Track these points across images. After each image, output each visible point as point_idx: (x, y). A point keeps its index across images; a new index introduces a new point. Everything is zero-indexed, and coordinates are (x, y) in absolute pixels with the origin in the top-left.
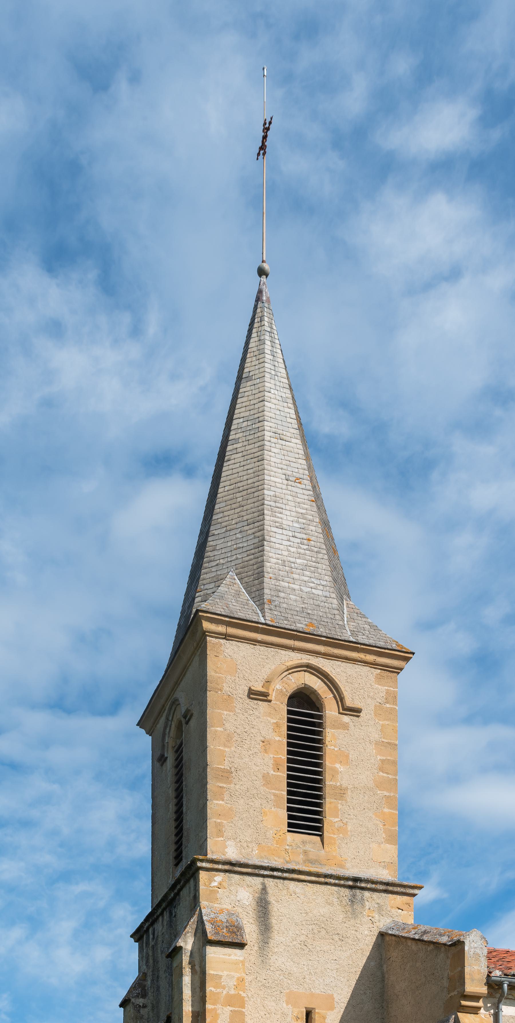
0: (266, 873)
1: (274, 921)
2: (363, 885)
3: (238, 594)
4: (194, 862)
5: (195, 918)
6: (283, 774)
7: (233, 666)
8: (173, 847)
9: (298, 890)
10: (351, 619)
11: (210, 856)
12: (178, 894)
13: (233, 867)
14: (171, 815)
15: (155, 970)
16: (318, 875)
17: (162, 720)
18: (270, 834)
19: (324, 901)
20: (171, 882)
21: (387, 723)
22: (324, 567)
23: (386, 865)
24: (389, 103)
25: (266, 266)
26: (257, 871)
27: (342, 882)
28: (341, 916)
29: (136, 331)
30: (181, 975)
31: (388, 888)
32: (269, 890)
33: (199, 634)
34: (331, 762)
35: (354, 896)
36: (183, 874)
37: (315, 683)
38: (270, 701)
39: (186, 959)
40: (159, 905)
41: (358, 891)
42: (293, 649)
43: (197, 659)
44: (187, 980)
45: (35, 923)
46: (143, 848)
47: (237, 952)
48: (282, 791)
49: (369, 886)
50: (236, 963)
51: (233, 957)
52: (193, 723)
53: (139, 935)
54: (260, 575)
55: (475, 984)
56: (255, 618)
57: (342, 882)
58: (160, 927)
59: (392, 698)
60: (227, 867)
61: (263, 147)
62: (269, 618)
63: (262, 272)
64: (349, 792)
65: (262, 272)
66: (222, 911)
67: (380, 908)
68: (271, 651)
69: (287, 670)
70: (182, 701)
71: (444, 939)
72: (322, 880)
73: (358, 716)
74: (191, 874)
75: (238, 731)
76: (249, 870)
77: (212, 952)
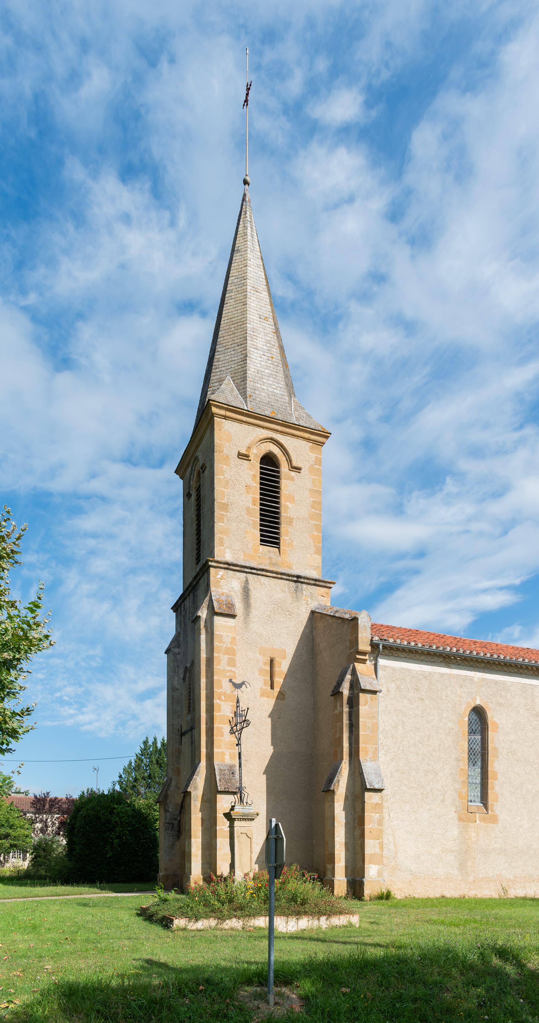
0: (248, 570)
1: (252, 601)
2: (302, 580)
3: (232, 390)
4: (207, 561)
5: (207, 598)
6: (258, 507)
7: (231, 437)
8: (195, 552)
9: (266, 583)
10: (296, 410)
11: (216, 559)
12: (198, 582)
13: (229, 566)
14: (194, 531)
16: (277, 573)
17: (189, 470)
20: (194, 574)
24: (315, 89)
25: (248, 179)
26: (242, 569)
27: (290, 578)
28: (290, 600)
29: (173, 223)
30: (200, 634)
31: (316, 583)
36: (201, 569)
37: (276, 450)
38: (250, 460)
39: (202, 624)
41: (299, 584)
44: (203, 637)
49: (306, 581)
51: (229, 624)
53: (176, 608)
54: (244, 379)
55: (364, 646)
57: (290, 578)
58: (188, 603)
59: (318, 461)
62: (250, 407)
63: (246, 182)
65: (246, 182)
66: (223, 594)
67: (312, 595)
70: (200, 458)
71: (347, 616)
72: (279, 576)
73: (300, 472)
74: (204, 570)
76: (238, 568)
77: (218, 620)
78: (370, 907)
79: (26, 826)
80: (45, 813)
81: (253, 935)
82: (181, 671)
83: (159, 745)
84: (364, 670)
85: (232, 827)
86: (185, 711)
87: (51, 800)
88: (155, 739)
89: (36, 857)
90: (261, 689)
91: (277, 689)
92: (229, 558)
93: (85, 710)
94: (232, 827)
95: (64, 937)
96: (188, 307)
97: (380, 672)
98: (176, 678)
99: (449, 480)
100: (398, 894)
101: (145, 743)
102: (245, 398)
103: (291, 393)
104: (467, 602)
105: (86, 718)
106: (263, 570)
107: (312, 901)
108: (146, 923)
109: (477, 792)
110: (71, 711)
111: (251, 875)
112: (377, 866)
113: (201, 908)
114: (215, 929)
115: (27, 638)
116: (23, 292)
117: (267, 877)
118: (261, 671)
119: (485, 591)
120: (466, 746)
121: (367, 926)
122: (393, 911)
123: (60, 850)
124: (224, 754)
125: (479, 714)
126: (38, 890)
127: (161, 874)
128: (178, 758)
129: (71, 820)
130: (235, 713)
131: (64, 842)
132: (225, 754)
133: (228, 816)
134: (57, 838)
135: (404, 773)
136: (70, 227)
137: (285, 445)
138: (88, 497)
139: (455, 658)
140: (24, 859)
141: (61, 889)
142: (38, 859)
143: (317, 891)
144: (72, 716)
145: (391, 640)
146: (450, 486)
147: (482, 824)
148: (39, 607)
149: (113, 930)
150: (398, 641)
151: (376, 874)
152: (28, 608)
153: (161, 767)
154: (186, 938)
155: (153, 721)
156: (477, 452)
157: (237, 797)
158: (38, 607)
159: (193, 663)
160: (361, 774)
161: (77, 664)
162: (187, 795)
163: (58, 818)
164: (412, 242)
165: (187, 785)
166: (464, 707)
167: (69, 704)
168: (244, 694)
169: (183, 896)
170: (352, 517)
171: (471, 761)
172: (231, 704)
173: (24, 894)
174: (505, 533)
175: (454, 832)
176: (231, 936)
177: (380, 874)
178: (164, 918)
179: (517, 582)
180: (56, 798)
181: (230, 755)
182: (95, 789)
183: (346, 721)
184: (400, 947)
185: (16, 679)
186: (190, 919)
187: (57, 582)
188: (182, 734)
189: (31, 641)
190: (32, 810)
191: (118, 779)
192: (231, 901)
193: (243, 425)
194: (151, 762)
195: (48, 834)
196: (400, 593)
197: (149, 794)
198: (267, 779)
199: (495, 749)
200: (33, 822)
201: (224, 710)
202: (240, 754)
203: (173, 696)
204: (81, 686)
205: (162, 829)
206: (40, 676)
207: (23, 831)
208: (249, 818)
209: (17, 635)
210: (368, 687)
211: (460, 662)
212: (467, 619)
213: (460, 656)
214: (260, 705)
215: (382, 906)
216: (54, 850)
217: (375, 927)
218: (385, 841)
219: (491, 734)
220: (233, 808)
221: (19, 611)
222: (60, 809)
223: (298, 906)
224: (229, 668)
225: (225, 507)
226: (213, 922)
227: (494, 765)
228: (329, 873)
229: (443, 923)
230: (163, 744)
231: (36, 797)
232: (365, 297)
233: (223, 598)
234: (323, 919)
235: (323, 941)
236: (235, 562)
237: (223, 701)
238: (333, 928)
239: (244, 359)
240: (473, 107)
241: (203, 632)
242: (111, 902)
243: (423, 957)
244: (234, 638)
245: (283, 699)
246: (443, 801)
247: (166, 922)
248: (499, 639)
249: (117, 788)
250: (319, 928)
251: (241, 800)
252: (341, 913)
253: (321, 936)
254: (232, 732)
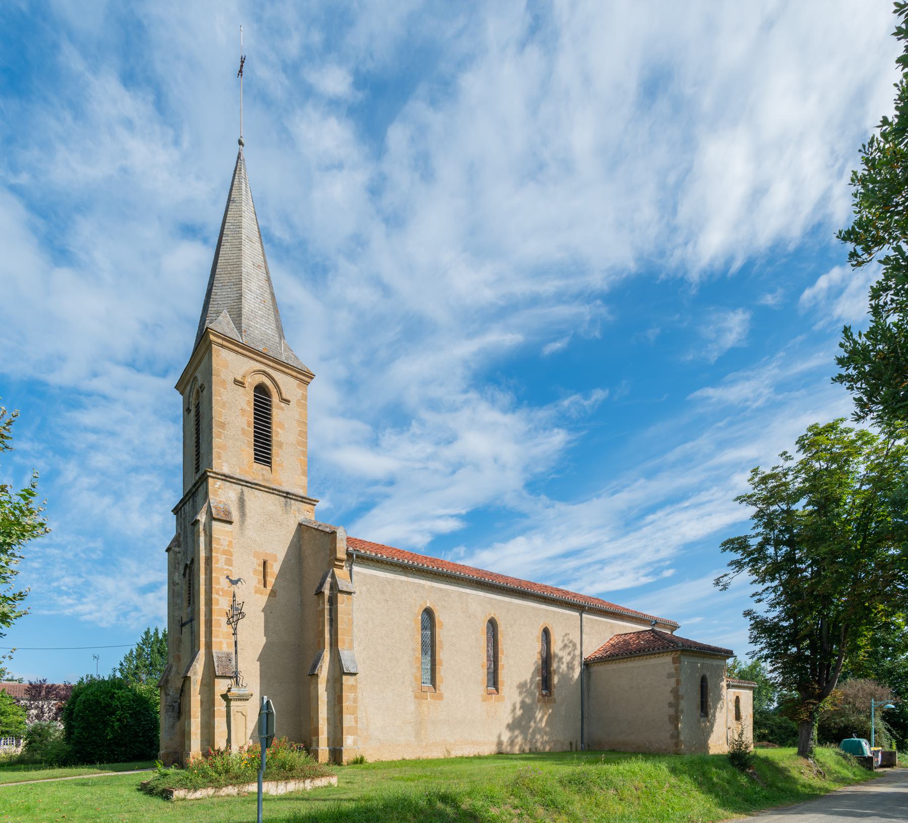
1: (247, 511)
3: (228, 323)
4: (206, 472)
5: (206, 505)
6: (252, 430)
7: (227, 365)
8: (195, 462)
10: (285, 350)
11: (214, 470)
12: (197, 489)
13: (226, 478)
14: (193, 444)
15: (185, 532)
16: (269, 488)
17: (189, 388)
18: (245, 462)
19: (273, 503)
20: (194, 482)
22: (272, 318)
23: (303, 488)
24: (311, 56)
25: (243, 140)
28: (280, 513)
29: (177, 142)
30: (199, 536)
31: (303, 499)
33: (208, 342)
34: (275, 427)
36: (200, 478)
37: (268, 383)
39: (201, 527)
40: (187, 495)
43: (207, 355)
44: (202, 539)
45: (118, 496)
46: (179, 459)
47: (228, 525)
48: (252, 440)
50: (228, 532)
52: (205, 392)
53: (177, 511)
54: (240, 315)
55: (341, 555)
56: (237, 339)
58: (187, 507)
59: (305, 397)
61: (241, 71)
62: (244, 340)
63: (240, 143)
65: (240, 143)
66: (220, 502)
67: (299, 510)
70: (199, 378)
71: (328, 530)
74: (204, 479)
77: (215, 524)
78: (347, 770)
79: (20, 713)
80: (41, 700)
81: (244, 799)
82: (182, 568)
83: (160, 636)
84: (341, 574)
85: (228, 706)
86: (185, 604)
87: (47, 687)
88: (157, 630)
89: (30, 743)
90: (255, 587)
91: (269, 588)
92: (226, 470)
93: (84, 600)
94: (228, 706)
95: (60, 815)
96: (189, 231)
97: (354, 577)
98: (177, 574)
99: (414, 423)
100: (369, 759)
101: (147, 633)
102: (240, 332)
103: (281, 336)
104: (427, 525)
105: (87, 609)
106: (257, 484)
107: (298, 767)
108: (147, 797)
109: (428, 676)
110: (70, 601)
111: (246, 748)
113: (200, 780)
114: (213, 797)
115: (19, 524)
116: (14, 169)
117: (259, 749)
118: (255, 571)
119: (440, 517)
120: (420, 639)
121: (344, 785)
122: (365, 772)
123: (57, 734)
124: (222, 643)
125: (429, 614)
126: (33, 774)
127: (162, 752)
128: (179, 646)
129: (69, 705)
130: (232, 607)
131: (62, 727)
133: (225, 697)
134: (55, 723)
136: (68, 115)
137: (276, 379)
138: (89, 394)
140: (17, 746)
141: (58, 771)
142: (33, 744)
143: (303, 758)
144: (71, 605)
145: (363, 551)
146: (415, 428)
148: (34, 495)
149: (113, 805)
150: (368, 552)
152: (21, 495)
153: (162, 655)
154: (185, 808)
155: (156, 612)
156: (434, 405)
157: (233, 681)
158: (32, 494)
159: (192, 561)
160: (340, 660)
161: (76, 555)
162: (186, 679)
163: (55, 704)
164: (387, 221)
165: (187, 671)
167: (67, 594)
168: (239, 589)
169: (182, 771)
170: (336, 445)
171: (424, 652)
173: (17, 779)
174: (454, 472)
175: (412, 707)
176: (227, 802)
177: (355, 742)
178: (164, 790)
179: (464, 512)
180: (53, 685)
182: (95, 676)
183: (327, 617)
184: (369, 800)
185: (7, 563)
186: (189, 789)
187: (53, 474)
188: (183, 625)
189: (24, 527)
190: (28, 696)
191: (119, 667)
192: (227, 772)
194: (153, 651)
195: (45, 720)
196: (375, 511)
197: (150, 680)
198: (261, 666)
199: (441, 642)
200: (27, 709)
201: (222, 604)
202: (236, 642)
203: (174, 590)
204: (80, 576)
205: (163, 712)
206: (35, 565)
207: (16, 717)
208: (244, 698)
209: (8, 520)
210: (345, 589)
212: (427, 539)
213: (415, 568)
214: (254, 601)
215: (357, 769)
216: (51, 735)
217: (350, 786)
218: (359, 716)
219: (437, 630)
220: (229, 690)
221: (10, 497)
222: (57, 695)
223: (286, 772)
224: (226, 567)
225: (223, 425)
226: (211, 791)
227: (441, 655)
228: (314, 744)
229: (402, 779)
230: (164, 635)
231: (31, 684)
232: (351, 256)
233: (221, 506)
234: (308, 781)
235: (307, 800)
238: (315, 789)
239: (240, 298)
240: (436, 119)
241: (202, 535)
242: (112, 780)
243: (386, 806)
244: (230, 542)
245: (275, 596)
246: (403, 683)
247: (166, 795)
248: (448, 557)
249: (118, 675)
250: (305, 789)
251: (237, 683)
252: (322, 776)
253: (306, 796)
254: (229, 623)
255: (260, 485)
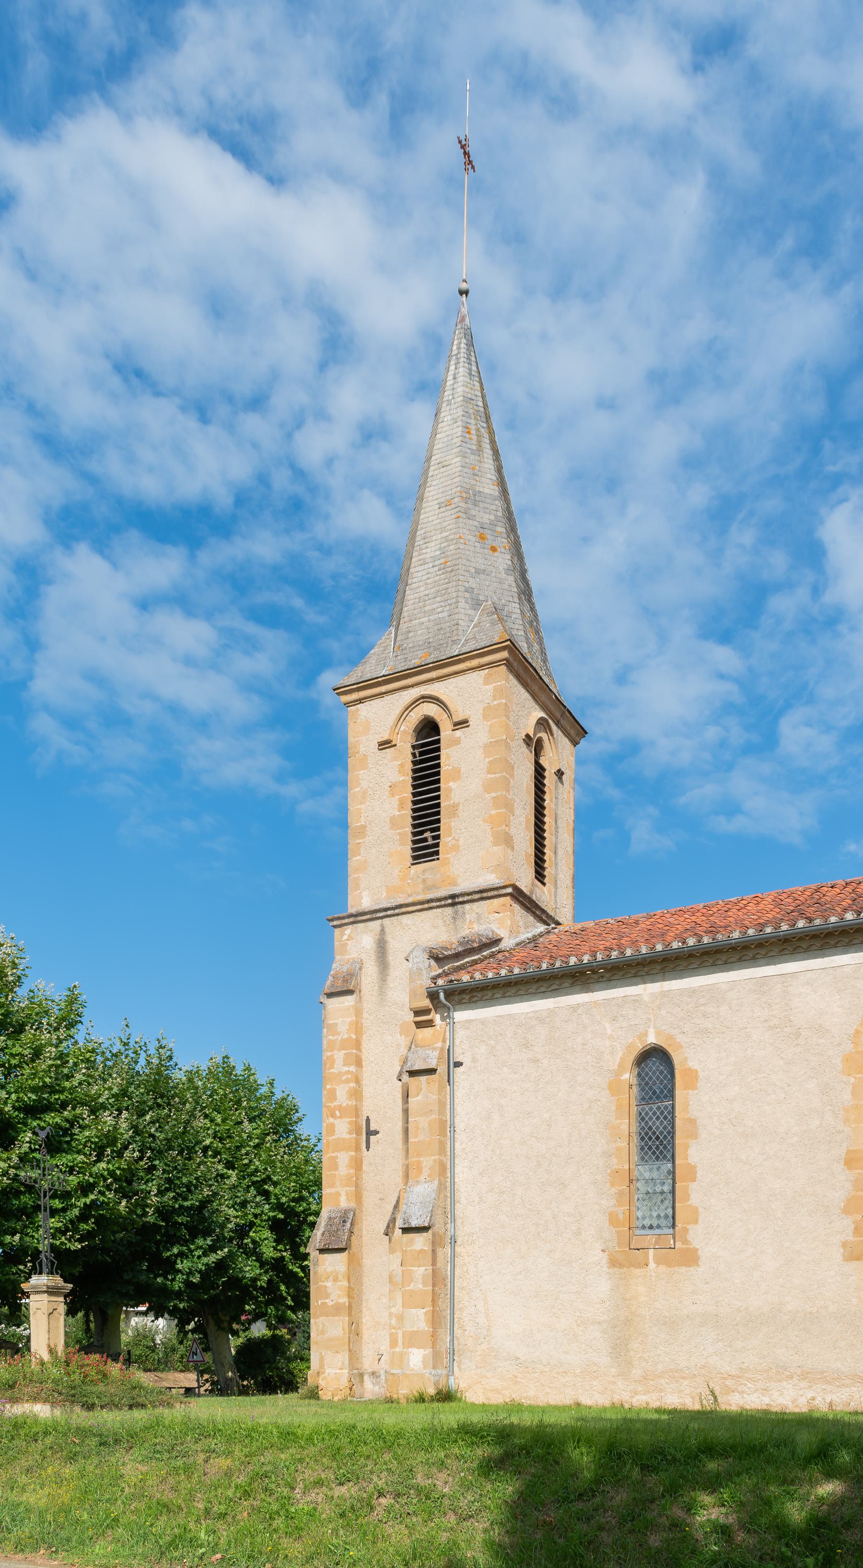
0: (381, 914)
2: (461, 899)
9: (409, 922)
21: (495, 720)
26: (374, 916)
27: (443, 903)
32: (387, 930)
35: (456, 913)
37: (430, 710)
38: (395, 745)
41: (459, 906)
42: (412, 686)
49: (466, 898)
51: (346, 1004)
57: (443, 903)
60: (351, 920)
64: (461, 807)
68: (388, 698)
69: (407, 709)
72: (426, 906)
73: (468, 726)
75: (371, 785)
76: (368, 917)
106: (400, 906)
112: (422, 1351)
132: (340, 1194)
135: (503, 1192)
137: (443, 698)
139: (594, 972)
147: (663, 1268)
151: (420, 1364)
166: (620, 1054)
172: (349, 1120)
181: (347, 1195)
193: (386, 698)
211: (608, 975)
236: (377, 907)
237: (339, 1118)
255: (407, 905)
